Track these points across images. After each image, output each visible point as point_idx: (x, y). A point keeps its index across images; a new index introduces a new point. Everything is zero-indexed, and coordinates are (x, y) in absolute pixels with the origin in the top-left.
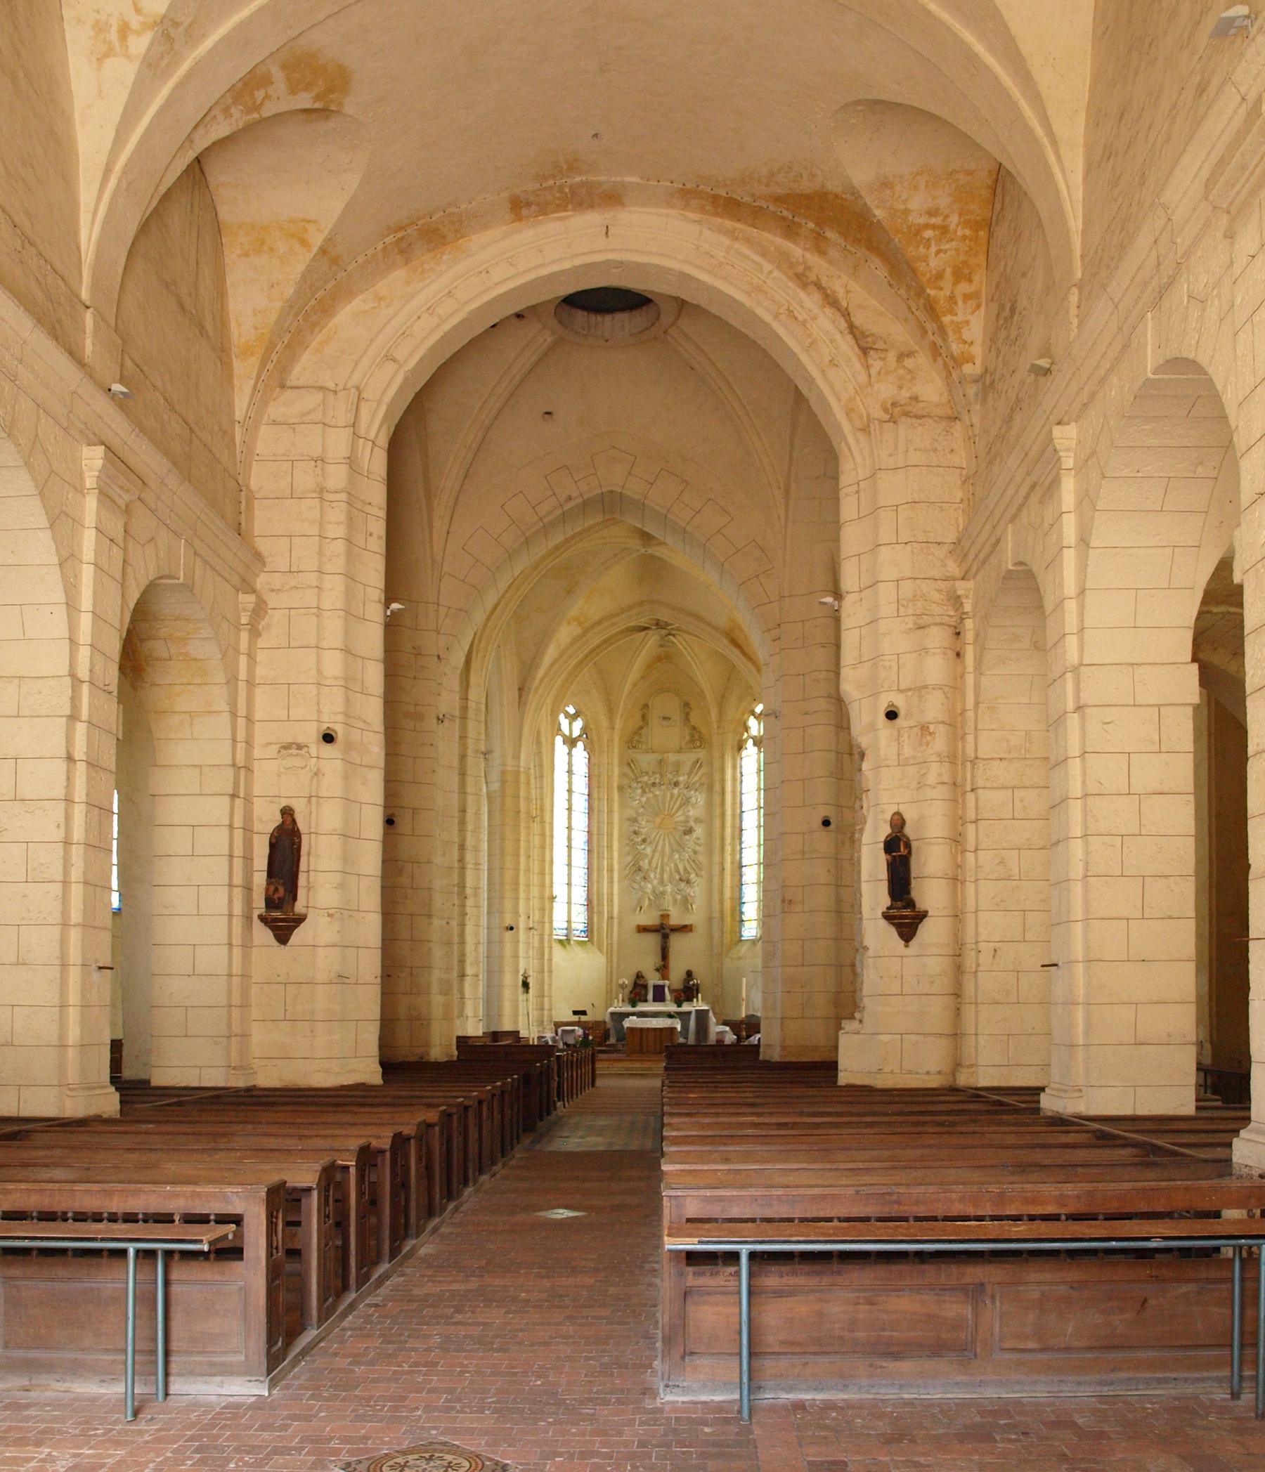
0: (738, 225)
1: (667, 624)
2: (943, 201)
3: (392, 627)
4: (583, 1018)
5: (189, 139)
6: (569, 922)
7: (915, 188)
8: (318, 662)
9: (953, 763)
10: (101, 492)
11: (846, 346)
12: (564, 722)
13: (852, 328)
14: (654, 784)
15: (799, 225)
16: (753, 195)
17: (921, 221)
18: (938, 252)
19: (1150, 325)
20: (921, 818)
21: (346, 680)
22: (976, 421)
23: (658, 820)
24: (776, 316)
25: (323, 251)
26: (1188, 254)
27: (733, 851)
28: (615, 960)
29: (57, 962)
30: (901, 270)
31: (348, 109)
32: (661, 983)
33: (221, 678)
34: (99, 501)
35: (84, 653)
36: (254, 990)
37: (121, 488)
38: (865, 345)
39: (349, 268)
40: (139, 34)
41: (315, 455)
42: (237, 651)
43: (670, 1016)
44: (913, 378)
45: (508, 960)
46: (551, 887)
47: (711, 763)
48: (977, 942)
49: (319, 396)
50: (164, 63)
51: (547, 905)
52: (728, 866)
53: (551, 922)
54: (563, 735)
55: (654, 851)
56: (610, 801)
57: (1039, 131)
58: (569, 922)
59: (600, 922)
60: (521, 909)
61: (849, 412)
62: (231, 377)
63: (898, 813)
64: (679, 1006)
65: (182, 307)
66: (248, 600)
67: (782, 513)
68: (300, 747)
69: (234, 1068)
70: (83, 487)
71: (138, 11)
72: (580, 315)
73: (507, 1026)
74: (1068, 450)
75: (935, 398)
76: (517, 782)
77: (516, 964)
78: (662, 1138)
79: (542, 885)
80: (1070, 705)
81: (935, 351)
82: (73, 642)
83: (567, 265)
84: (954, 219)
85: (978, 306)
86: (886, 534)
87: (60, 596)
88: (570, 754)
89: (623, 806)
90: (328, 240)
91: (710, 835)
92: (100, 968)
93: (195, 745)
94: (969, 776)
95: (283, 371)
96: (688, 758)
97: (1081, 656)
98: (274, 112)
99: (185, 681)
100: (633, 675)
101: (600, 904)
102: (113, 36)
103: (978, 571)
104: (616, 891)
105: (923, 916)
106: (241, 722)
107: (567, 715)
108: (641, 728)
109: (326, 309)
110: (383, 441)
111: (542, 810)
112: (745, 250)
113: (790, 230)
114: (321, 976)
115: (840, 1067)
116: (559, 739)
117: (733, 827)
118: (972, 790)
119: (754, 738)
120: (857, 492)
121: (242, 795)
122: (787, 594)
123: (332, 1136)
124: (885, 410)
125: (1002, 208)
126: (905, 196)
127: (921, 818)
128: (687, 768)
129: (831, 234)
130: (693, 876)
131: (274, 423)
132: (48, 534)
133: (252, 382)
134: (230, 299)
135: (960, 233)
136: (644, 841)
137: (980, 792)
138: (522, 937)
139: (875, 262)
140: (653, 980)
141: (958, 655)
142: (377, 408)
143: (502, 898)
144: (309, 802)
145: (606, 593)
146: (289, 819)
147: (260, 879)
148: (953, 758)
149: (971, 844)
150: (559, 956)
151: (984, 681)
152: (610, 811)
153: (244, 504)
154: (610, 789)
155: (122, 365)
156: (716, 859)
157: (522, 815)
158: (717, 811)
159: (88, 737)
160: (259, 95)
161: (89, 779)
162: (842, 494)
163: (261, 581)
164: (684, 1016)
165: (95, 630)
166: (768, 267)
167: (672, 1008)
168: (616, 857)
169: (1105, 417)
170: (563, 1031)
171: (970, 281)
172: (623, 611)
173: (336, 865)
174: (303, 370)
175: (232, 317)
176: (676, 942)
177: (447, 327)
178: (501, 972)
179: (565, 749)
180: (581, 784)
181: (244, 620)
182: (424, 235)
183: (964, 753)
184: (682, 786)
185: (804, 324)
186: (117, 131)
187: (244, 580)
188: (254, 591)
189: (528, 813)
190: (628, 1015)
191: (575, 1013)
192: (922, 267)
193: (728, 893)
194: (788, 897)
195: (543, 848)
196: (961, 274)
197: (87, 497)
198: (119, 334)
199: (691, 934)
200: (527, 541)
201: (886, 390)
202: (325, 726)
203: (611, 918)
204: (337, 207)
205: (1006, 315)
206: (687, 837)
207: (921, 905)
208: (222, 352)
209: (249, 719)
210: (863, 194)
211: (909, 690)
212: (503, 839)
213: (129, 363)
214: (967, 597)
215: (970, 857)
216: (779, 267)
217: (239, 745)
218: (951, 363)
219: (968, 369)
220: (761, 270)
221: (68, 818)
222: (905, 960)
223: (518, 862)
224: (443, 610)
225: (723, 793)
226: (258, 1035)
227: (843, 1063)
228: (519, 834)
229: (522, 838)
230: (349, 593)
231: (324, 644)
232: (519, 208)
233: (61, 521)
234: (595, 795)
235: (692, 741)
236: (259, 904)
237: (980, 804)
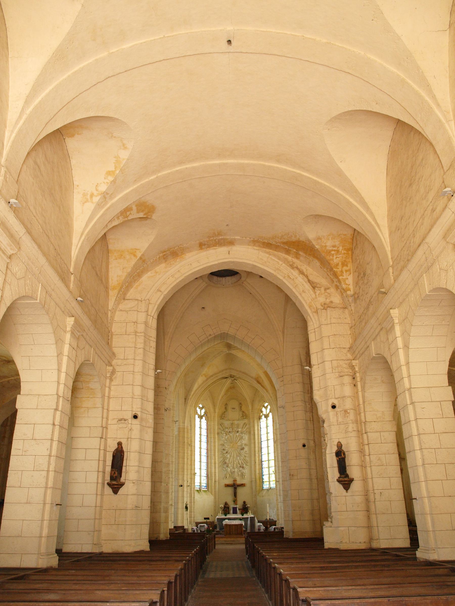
0: (271, 251)
1: (234, 376)
2: (337, 243)
3: (157, 377)
4: (208, 520)
5: (107, 226)
6: (200, 483)
7: (328, 239)
8: (133, 390)
9: (357, 423)
10: (72, 332)
11: (308, 286)
13: (309, 281)
15: (291, 250)
16: (276, 242)
17: (331, 249)
18: (336, 258)
19: (425, 278)
20: (348, 444)
21: (142, 396)
22: (353, 308)
23: (232, 445)
24: (284, 277)
25: (141, 258)
26: (437, 257)
27: (259, 455)
28: (217, 497)
29: (42, 502)
30: (324, 263)
31: (154, 217)
32: (235, 506)
33: (100, 395)
34: (71, 335)
35: (62, 387)
36: (104, 512)
37: (78, 331)
38: (314, 286)
39: (148, 263)
40: (96, 196)
41: (134, 321)
42: (105, 386)
43: (240, 519)
44: (330, 296)
45: (180, 498)
46: (194, 470)
48: (373, 490)
49: (136, 302)
50: (102, 204)
51: (193, 477)
52: (257, 461)
53: (194, 483)
54: (198, 415)
55: (230, 456)
56: (214, 438)
57: (373, 223)
58: (200, 483)
60: (185, 478)
61: (310, 307)
62: (108, 296)
63: (339, 442)
64: (243, 515)
65: (97, 274)
66: (110, 368)
67: (282, 339)
68: (125, 420)
69: (95, 544)
70: (66, 331)
71: (97, 190)
72: (215, 278)
73: (180, 524)
74: (396, 317)
75: (338, 302)
76: (184, 431)
79: (191, 469)
80: (409, 402)
81: (337, 287)
82: (58, 383)
83: (216, 263)
84: (341, 248)
85: (350, 274)
86: (326, 346)
87: (56, 367)
88: (200, 421)
89: (219, 440)
90: (143, 255)
91: (250, 449)
92: (57, 505)
93: (90, 420)
94: (363, 428)
95: (125, 294)
96: (241, 423)
97: (411, 385)
98: (132, 218)
99: (87, 396)
100: (223, 393)
102: (88, 197)
103: (360, 357)
104: (217, 471)
105: (352, 480)
106: (105, 411)
107: (200, 408)
108: (225, 412)
109: (139, 276)
110: (156, 317)
111: (191, 441)
112: (274, 258)
113: (288, 252)
114: (130, 507)
115: (325, 541)
116: (197, 416)
117: (258, 447)
118: (365, 433)
119: (264, 415)
120: (315, 332)
121: (104, 437)
122: (285, 366)
123: (151, 576)
124: (322, 306)
125: (356, 245)
126: (325, 242)
127: (348, 444)
129: (301, 253)
131: (121, 310)
132: (55, 346)
133: (115, 298)
134: (110, 272)
135: (343, 252)
136: (227, 452)
137: (368, 433)
138: (185, 490)
139: (316, 261)
140: (232, 505)
141: (355, 385)
142: (154, 306)
144: (128, 440)
145: (214, 367)
146: (120, 446)
147: (108, 469)
148: (357, 421)
149: (367, 453)
150: (197, 496)
151: (366, 394)
152: (215, 442)
153: (110, 336)
154: (214, 434)
155: (80, 292)
156: (253, 459)
157: (186, 443)
158: (253, 441)
159: (61, 417)
160: (128, 213)
161: (60, 432)
162: (309, 333)
163: (114, 362)
165: (66, 379)
166: (281, 263)
168: (217, 459)
169: (410, 306)
170: (200, 526)
171: (347, 266)
172: (220, 372)
173: (137, 464)
174: (131, 293)
175: (110, 277)
176: (240, 491)
177: (178, 281)
180: (204, 432)
181: (108, 375)
182: (171, 253)
183: (360, 420)
185: (293, 280)
186: (87, 223)
187: (109, 362)
188: (112, 366)
189: (188, 443)
190: (224, 519)
191: (205, 519)
192: (331, 262)
193: (257, 472)
194: (292, 473)
195: (191, 455)
196: (344, 264)
197: (67, 334)
198: (80, 282)
200: (196, 349)
201: (322, 299)
202: (134, 413)
203: (215, 481)
204: (146, 245)
205: (361, 275)
207: (351, 476)
208: (107, 288)
209: (108, 410)
210: (312, 241)
211: (339, 398)
213: (82, 291)
214: (356, 366)
215: (367, 457)
216: (284, 263)
217: (104, 419)
218: (343, 291)
219: (349, 293)
220: (279, 264)
221: (51, 446)
222: (347, 498)
223: (184, 461)
224: (167, 372)
225: (254, 435)
226: (104, 530)
227: (326, 539)
229: (186, 452)
230: (144, 367)
231: (134, 384)
232: (202, 246)
233: (59, 341)
234: (209, 436)
235: (243, 416)
236: (108, 478)
237: (369, 438)
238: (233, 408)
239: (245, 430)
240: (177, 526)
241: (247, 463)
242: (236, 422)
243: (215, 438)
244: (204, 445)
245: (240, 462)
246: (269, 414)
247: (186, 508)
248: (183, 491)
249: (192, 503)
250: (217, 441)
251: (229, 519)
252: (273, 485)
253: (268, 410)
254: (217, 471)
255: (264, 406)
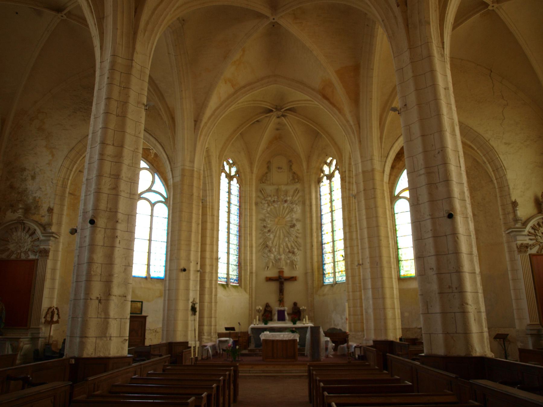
6: (228, 274)
12: (227, 168)
14: (274, 201)
23: (276, 220)
28: (254, 296)
32: (282, 309)
43: (293, 330)
47: (303, 191)
52: (315, 244)
54: (226, 173)
55: (275, 237)
56: (251, 209)
58: (228, 274)
59: (245, 274)
64: (294, 323)
76: (192, 176)
77: (188, 294)
78: (226, 278)
79: (212, 251)
89: (258, 213)
91: (304, 228)
96: (291, 188)
101: (246, 265)
107: (228, 163)
108: (267, 173)
116: (223, 175)
117: (317, 223)
119: (326, 175)
128: (291, 193)
130: (296, 250)
136: (269, 231)
140: (276, 308)
143: (179, 250)
152: (251, 215)
156: (308, 240)
158: (308, 215)
164: (303, 330)
167: (289, 325)
168: (254, 240)
176: (289, 287)
178: (177, 300)
179: (227, 180)
180: (235, 200)
184: (289, 202)
191: (227, 329)
199: (295, 283)
203: (251, 273)
206: (292, 229)
212: (181, 211)
223: (191, 227)
225: (311, 205)
228: (192, 208)
234: (243, 207)
235: (294, 179)
238: (279, 168)
239: (296, 198)
240: (174, 341)
241: (300, 246)
242: (283, 188)
243: (252, 209)
244: (235, 219)
245: (289, 245)
246: (334, 172)
247: (194, 309)
248: (188, 280)
249: (213, 304)
250: (254, 214)
251: (272, 330)
252: (341, 277)
253: (333, 167)
254: (254, 258)
255: (326, 163)
